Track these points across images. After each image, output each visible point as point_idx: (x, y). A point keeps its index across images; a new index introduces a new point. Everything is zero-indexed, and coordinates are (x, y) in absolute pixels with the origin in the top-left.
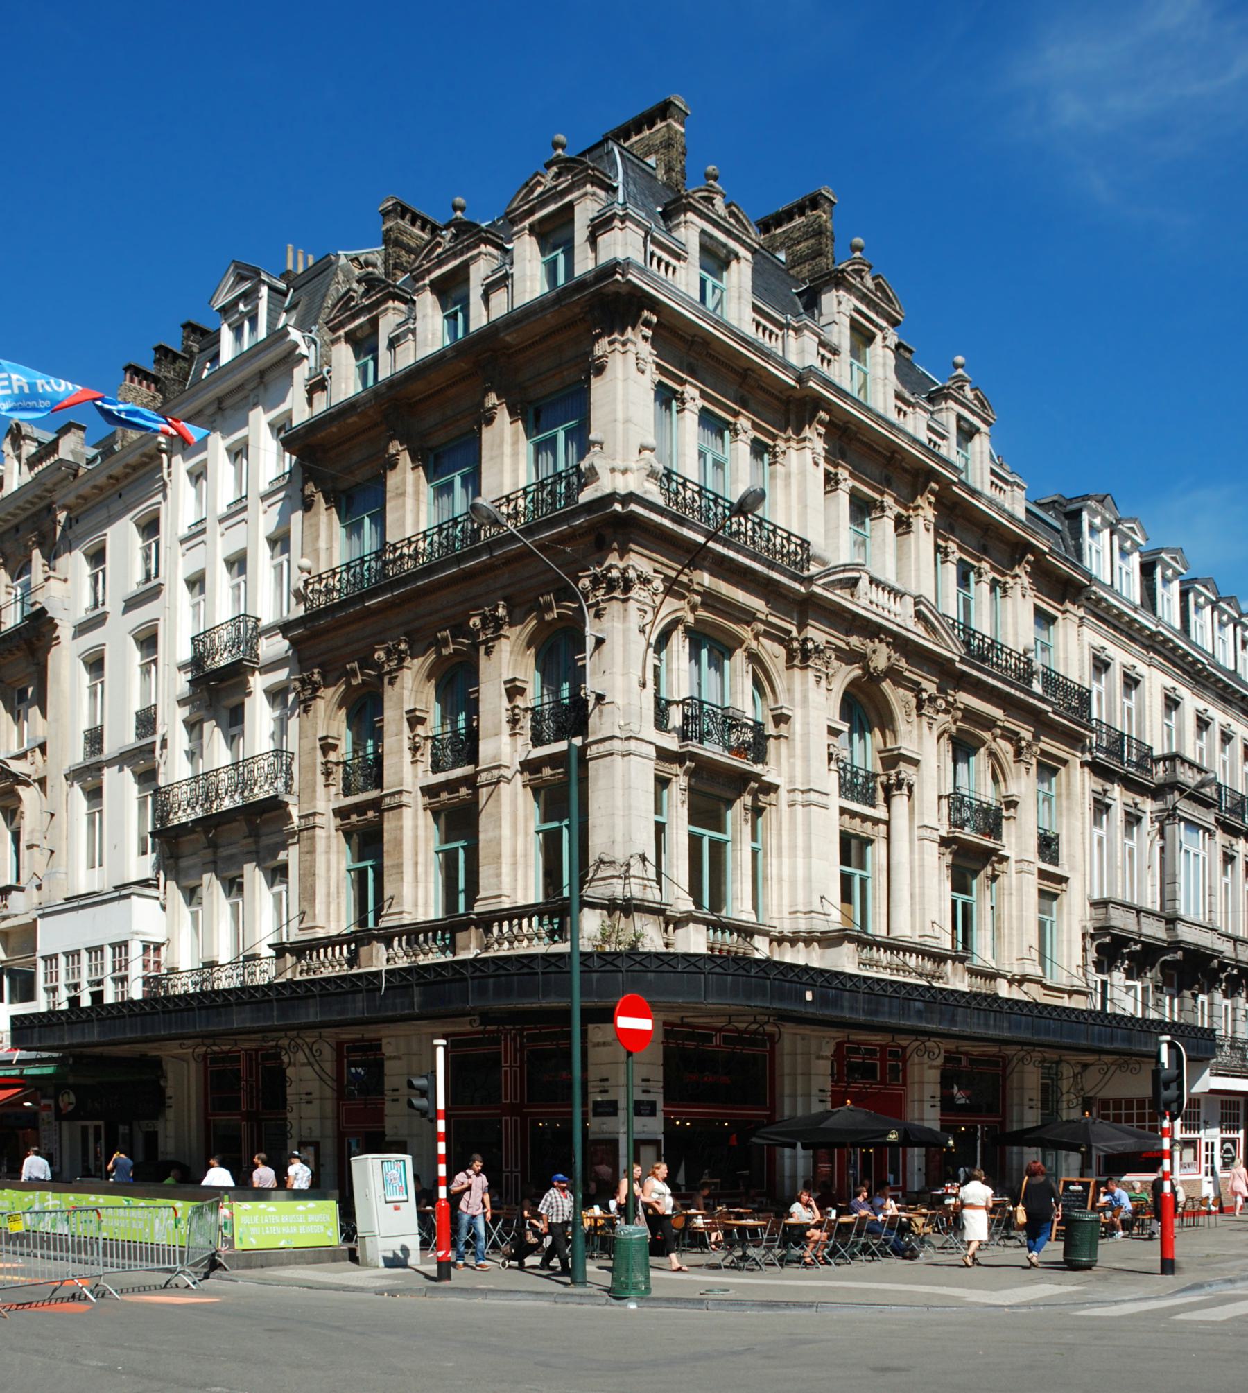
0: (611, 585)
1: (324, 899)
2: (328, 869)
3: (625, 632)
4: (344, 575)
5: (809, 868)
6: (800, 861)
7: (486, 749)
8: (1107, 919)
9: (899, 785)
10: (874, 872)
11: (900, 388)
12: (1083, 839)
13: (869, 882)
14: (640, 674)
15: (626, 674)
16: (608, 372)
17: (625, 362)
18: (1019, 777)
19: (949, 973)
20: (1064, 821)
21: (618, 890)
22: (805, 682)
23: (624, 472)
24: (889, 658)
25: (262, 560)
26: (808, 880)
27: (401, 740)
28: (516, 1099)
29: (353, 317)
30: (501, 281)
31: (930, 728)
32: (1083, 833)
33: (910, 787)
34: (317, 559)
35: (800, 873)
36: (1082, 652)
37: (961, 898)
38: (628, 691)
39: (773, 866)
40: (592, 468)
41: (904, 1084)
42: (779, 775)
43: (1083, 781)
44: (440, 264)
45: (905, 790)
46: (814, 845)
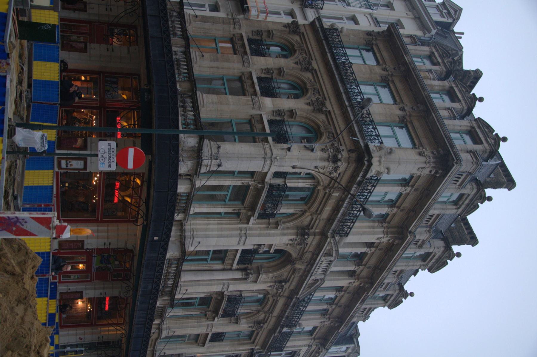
5: (213, 237)
10: (209, 264)
18: (248, 323)
19: (163, 298)
20: (229, 343)
22: (291, 234)
24: (300, 269)
26: (207, 237)
33: (246, 279)
41: (112, 280)
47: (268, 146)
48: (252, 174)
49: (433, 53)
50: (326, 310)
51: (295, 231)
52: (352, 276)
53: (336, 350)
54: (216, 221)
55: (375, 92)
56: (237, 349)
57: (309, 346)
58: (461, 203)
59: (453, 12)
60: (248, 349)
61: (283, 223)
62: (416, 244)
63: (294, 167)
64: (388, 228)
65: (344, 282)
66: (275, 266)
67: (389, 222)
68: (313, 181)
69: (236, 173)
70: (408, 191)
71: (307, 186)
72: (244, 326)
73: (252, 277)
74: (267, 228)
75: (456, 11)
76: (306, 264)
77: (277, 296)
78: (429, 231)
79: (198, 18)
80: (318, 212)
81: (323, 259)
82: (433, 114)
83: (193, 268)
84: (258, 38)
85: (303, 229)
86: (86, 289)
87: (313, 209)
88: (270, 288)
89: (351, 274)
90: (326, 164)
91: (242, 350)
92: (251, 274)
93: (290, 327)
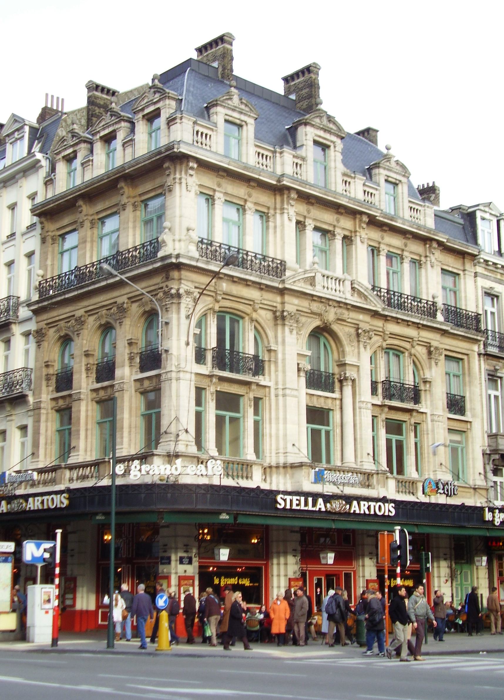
0: (172, 296)
1: (44, 446)
2: (46, 431)
3: (179, 319)
4: (57, 281)
5: (285, 429)
6: (281, 426)
7: (118, 373)
8: (497, 444)
9: (346, 379)
10: (333, 428)
11: (345, 169)
12: (482, 398)
13: (331, 433)
14: (186, 339)
15: (179, 340)
16: (173, 192)
17: (181, 187)
18: (430, 367)
19: (375, 483)
20: (467, 388)
21: (171, 447)
22: (283, 332)
23: (180, 241)
24: (336, 314)
25: (22, 264)
26: (285, 435)
27: (81, 366)
28: (129, 554)
29: (65, 149)
30: (129, 143)
31: (365, 348)
32: (481, 395)
33: (353, 381)
34: (46, 270)
35: (281, 433)
36: (477, 292)
37: (394, 438)
38: (179, 348)
39: (267, 429)
40: (164, 242)
41: (354, 545)
42: (270, 381)
43: (480, 365)
44: (104, 129)
45: (350, 383)
46: (288, 417)
47: (164, 375)
48: (199, 391)
49: (63, 157)
50: (413, 261)
51: (280, 328)
52: (352, 241)
53: (486, 235)
54: (267, 425)
55: (108, 237)
56: (478, 377)
57: (476, 276)
58: (238, 122)
59: (17, 124)
60: (479, 360)
61: (269, 344)
62: (301, 165)
63: (188, 344)
64: (275, 209)
65: (361, 251)
66: (335, 343)
67: (269, 208)
68: (208, 315)
69: (199, 409)
70: (221, 195)
71: (216, 323)
72: (437, 374)
73: (350, 373)
74: (276, 362)
75: (16, 121)
76: (328, 307)
77: (382, 334)
78: (281, 153)
79: (35, 452)
80: (251, 303)
81: (319, 287)
82: (127, 171)
83: (339, 448)
84: (54, 379)
85: (276, 318)
86: (364, 577)
87: (248, 309)
88: (368, 347)
89: (348, 240)
90: (183, 306)
91: (480, 369)
92: (345, 374)
93: (436, 310)
